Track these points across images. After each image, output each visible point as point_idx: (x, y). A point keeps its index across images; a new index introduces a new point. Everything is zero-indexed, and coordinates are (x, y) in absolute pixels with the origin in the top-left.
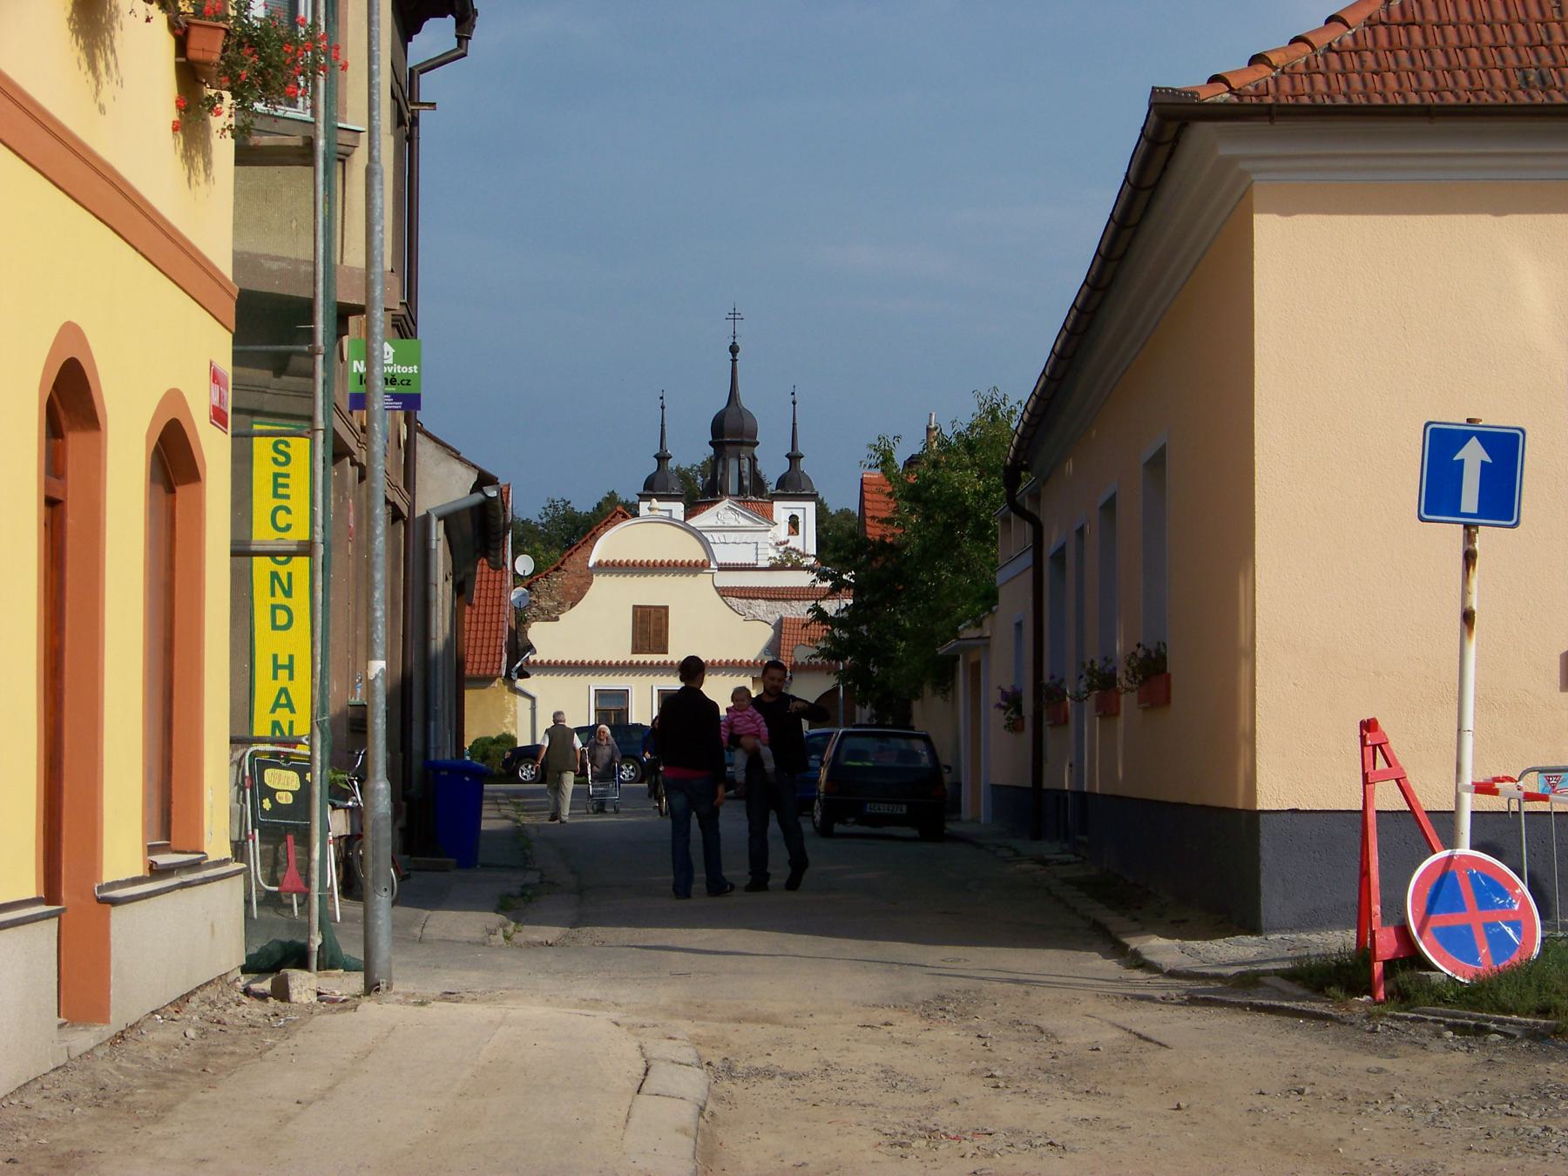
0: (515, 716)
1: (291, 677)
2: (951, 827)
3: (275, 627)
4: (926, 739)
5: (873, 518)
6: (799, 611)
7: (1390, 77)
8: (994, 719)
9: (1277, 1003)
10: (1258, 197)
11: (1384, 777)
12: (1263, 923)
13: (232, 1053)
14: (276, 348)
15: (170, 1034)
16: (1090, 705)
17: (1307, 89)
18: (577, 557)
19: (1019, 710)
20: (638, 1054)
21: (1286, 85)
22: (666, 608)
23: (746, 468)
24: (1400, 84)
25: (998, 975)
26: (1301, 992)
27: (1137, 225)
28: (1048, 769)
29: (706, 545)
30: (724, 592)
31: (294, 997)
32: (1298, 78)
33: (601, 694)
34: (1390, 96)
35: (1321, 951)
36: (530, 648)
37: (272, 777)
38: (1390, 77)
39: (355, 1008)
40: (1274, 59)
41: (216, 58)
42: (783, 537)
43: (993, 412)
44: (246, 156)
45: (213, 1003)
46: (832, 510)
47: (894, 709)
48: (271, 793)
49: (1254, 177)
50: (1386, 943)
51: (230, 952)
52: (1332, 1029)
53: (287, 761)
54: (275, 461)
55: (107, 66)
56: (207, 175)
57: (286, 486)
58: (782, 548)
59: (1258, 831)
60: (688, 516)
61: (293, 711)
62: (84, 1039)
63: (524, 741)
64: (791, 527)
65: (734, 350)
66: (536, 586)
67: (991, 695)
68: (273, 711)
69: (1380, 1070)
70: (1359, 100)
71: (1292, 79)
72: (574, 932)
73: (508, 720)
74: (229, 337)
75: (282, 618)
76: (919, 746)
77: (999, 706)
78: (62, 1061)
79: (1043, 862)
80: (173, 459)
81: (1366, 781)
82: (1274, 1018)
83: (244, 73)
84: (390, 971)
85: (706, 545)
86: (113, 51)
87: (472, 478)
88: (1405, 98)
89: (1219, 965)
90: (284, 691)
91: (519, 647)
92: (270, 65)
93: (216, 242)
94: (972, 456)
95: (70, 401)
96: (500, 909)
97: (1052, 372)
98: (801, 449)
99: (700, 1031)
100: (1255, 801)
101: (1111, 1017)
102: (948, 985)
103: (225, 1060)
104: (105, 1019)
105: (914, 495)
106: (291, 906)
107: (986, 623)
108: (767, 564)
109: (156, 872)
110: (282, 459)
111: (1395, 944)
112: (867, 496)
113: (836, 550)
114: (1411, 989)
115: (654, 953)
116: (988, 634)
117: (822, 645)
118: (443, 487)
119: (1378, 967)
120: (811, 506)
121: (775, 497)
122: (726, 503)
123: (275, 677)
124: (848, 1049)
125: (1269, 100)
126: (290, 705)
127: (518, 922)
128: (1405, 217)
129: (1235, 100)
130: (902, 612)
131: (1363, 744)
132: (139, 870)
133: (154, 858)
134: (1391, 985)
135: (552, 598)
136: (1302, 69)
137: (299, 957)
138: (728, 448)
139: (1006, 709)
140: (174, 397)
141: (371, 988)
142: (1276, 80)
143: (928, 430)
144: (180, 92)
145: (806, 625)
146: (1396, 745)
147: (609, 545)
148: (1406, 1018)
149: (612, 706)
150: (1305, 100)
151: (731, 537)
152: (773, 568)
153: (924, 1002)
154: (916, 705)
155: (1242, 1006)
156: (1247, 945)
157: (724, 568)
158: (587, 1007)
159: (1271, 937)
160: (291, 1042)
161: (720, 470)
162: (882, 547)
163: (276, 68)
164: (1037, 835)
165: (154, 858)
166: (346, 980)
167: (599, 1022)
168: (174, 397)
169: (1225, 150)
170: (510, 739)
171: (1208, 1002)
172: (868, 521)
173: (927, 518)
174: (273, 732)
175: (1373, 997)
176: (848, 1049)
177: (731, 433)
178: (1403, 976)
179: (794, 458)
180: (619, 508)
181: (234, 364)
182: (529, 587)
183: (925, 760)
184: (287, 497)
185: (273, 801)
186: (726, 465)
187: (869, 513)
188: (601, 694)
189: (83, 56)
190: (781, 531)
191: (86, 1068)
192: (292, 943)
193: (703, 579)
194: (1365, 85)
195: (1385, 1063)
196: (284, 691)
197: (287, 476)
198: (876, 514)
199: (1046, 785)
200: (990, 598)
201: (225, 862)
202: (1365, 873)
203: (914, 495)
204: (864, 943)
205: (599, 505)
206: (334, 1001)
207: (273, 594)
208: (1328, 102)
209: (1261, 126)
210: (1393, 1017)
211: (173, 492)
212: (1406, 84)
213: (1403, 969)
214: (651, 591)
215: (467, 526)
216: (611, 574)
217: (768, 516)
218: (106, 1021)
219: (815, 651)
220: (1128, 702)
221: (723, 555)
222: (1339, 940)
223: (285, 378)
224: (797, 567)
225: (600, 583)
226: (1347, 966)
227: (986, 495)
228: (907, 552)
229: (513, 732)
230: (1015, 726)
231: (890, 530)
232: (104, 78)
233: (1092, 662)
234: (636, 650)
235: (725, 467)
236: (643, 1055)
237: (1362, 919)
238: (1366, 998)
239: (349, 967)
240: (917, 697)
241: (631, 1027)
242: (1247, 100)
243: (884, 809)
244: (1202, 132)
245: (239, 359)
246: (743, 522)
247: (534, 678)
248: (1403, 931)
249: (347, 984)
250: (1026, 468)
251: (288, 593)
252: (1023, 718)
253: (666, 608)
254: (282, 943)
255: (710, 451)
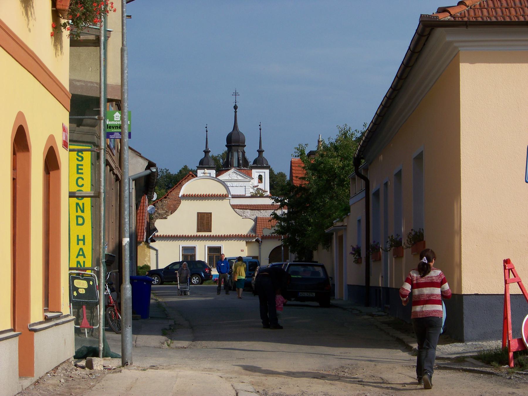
0: (150, 258)
1: (84, 244)
2: (332, 302)
3: (78, 224)
4: (323, 266)
5: (297, 177)
6: (267, 214)
7: (512, 10)
8: (349, 259)
9: (472, 368)
10: (461, 55)
11: (513, 281)
12: (465, 338)
13: (79, 388)
14: (79, 117)
15: (54, 381)
16: (390, 254)
17: (480, 15)
18: (173, 193)
19: (359, 255)
20: (232, 388)
21: (472, 13)
22: (211, 213)
23: (241, 156)
24: (516, 13)
25: (363, 358)
26: (481, 364)
27: (413, 66)
28: (372, 278)
29: (227, 187)
30: (234, 207)
31: (95, 368)
32: (476, 10)
33: (185, 249)
34: (512, 17)
35: (488, 348)
36: (155, 230)
37: (78, 283)
38: (512, 10)
39: (121, 371)
40: (467, 3)
41: (67, 8)
42: (256, 184)
43: (345, 134)
44: (74, 43)
45: (66, 370)
46: (276, 173)
47: (306, 255)
48: (77, 289)
49: (460, 49)
50: (514, 345)
51: (70, 351)
52: (494, 378)
53: (83, 277)
54: (77, 159)
55: (31, 14)
56: (61, 52)
57: (82, 169)
58: (255, 189)
59: (463, 302)
60: (217, 175)
61: (85, 257)
62: (27, 382)
63: (153, 268)
64: (259, 180)
65: (235, 107)
66: (157, 205)
67: (348, 249)
68: (77, 257)
69: (514, 393)
70: (500, 19)
71: (474, 11)
72: (194, 343)
73: (147, 259)
74: (68, 113)
75: (80, 221)
76: (319, 269)
77: (351, 253)
78: (20, 390)
79: (372, 315)
80: (51, 162)
81: (506, 281)
82: (472, 374)
83: (79, 14)
84: (132, 358)
85: (227, 187)
86: (33, 7)
87: (146, 164)
88: (518, 18)
89: (449, 354)
90: (81, 249)
91: (151, 230)
92: (87, 11)
93: (64, 77)
94: (337, 152)
95: (20, 141)
96: (164, 334)
97: (375, 121)
98: (263, 148)
99: (252, 380)
100: (461, 291)
101: (408, 374)
102: (343, 362)
103: (77, 391)
104: (32, 376)
105: (314, 168)
106: (85, 333)
107: (345, 220)
108: (249, 195)
109: (47, 319)
110: (80, 159)
111: (518, 345)
112: (293, 168)
113: (282, 190)
114: (524, 362)
115: (229, 351)
116: (346, 224)
117: (276, 228)
118: (135, 167)
119: (511, 354)
120: (267, 171)
121: (252, 168)
122: (233, 170)
123: (78, 244)
124: (310, 386)
125: (466, 19)
126: (83, 255)
127: (171, 339)
128: (519, 64)
129: (452, 19)
130: (309, 216)
131: (505, 268)
132: (42, 319)
133: (46, 314)
134: (516, 361)
135: (163, 209)
136: (478, 7)
137: (95, 353)
138: (233, 148)
139: (354, 254)
140: (51, 138)
141: (125, 364)
142: (468, 11)
143: (319, 141)
144: (53, 21)
145: (270, 221)
146: (518, 269)
147: (188, 188)
148: (522, 374)
149: (189, 254)
150: (480, 19)
151: (235, 184)
152: (252, 197)
153: (336, 369)
154: (315, 253)
155: (459, 370)
156: (459, 347)
157: (234, 197)
158: (207, 371)
159: (468, 343)
160: (101, 384)
161: (230, 157)
162: (301, 189)
163: (90, 12)
164: (368, 305)
165: (46, 314)
166: (112, 361)
167: (214, 377)
168: (51, 138)
169: (449, 39)
170: (148, 267)
171: (445, 368)
172: (294, 178)
173: (319, 177)
174: (77, 265)
175: (509, 365)
176: (310, 386)
177: (234, 141)
178: (521, 358)
179: (260, 152)
180: (191, 173)
181: (70, 123)
182: (154, 205)
183: (322, 275)
184: (82, 173)
185: (77, 292)
186: (232, 155)
187: (294, 175)
188: (185, 249)
189: (24, 11)
190: (255, 181)
191: (29, 393)
192: (90, 347)
193: (226, 202)
194: (503, 13)
195: (515, 390)
196: (81, 249)
197: (82, 165)
198: (297, 175)
199: (371, 285)
200: (347, 210)
201: (68, 316)
202: (506, 318)
203: (314, 168)
204: (309, 347)
205: (180, 171)
206: (110, 369)
207: (77, 212)
208: (489, 20)
209: (463, 29)
210: (517, 373)
211: (49, 173)
212: (519, 13)
213: (521, 355)
214: (204, 206)
215: (143, 183)
216: (188, 200)
217: (250, 176)
218: (33, 376)
219: (274, 231)
220: (407, 252)
221: (234, 191)
222: (496, 344)
223: (81, 127)
224: (262, 196)
225: (184, 204)
226: (499, 354)
227: (343, 168)
228: (311, 191)
229: (149, 264)
230: (358, 261)
231: (304, 182)
232: (30, 18)
233: (392, 236)
234: (198, 230)
235: (232, 156)
236: (234, 388)
237: (504, 336)
238: (506, 366)
239: (114, 356)
240: (316, 249)
241: (227, 378)
242: (457, 19)
243: (306, 294)
244: (439, 32)
245: (71, 121)
246: (240, 178)
247: (157, 242)
248: (521, 341)
249: (116, 363)
250: (363, 158)
251: (83, 211)
252: (361, 258)
253: (211, 213)
254: (87, 347)
255: (226, 149)
